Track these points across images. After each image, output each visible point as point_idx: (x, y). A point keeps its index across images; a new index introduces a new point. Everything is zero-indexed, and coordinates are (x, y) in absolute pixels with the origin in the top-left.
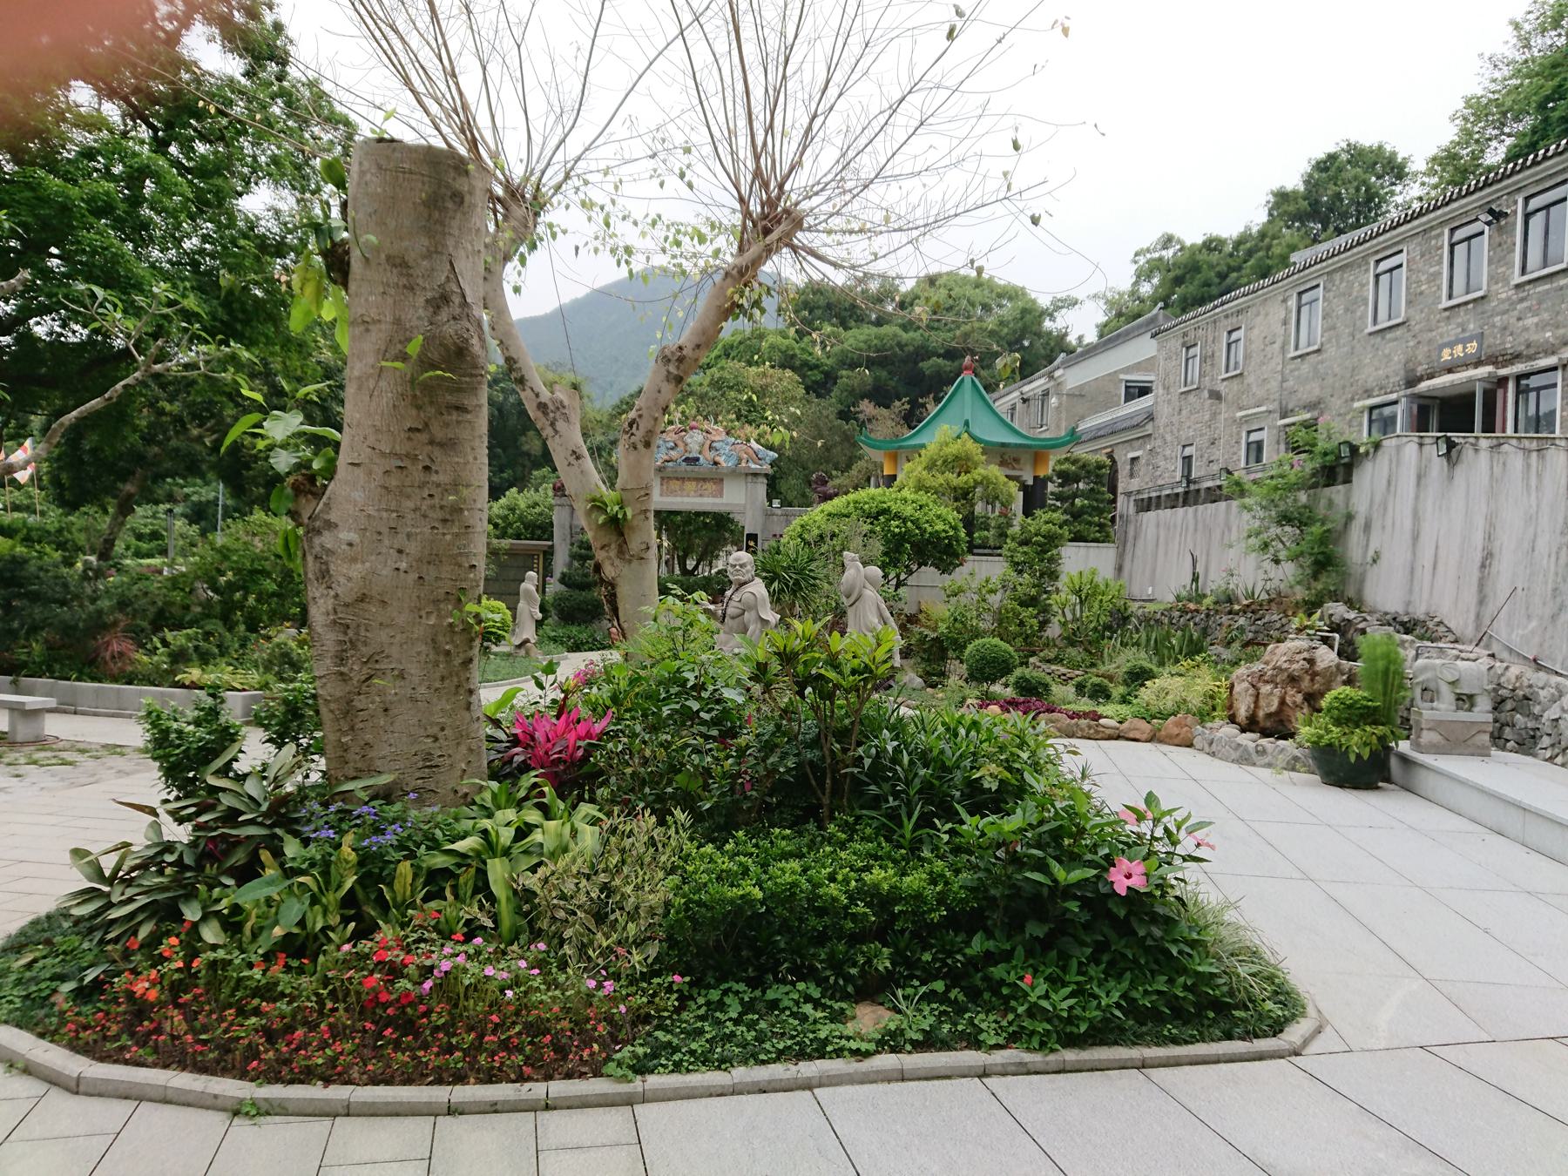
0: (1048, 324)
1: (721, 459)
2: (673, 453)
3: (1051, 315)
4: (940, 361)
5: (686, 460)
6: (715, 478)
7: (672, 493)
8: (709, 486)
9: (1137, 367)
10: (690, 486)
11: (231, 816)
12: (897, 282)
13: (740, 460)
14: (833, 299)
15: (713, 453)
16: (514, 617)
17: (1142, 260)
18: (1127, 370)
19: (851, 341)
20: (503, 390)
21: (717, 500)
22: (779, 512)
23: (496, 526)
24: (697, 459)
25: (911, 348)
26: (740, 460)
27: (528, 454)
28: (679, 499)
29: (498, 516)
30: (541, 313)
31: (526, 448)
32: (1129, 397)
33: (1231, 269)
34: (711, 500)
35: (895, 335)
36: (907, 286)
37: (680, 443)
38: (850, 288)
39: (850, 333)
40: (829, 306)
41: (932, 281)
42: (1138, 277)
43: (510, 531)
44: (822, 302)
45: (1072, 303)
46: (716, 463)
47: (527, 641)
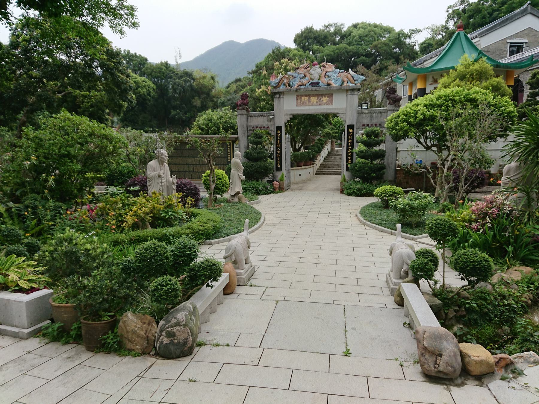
0: (407, 41)
1: (332, 82)
2: (304, 81)
3: (409, 37)
4: (364, 58)
5: (312, 84)
6: (329, 92)
7: (304, 104)
8: (325, 99)
9: (516, 35)
10: (314, 99)
11: (494, 328)
12: (342, 27)
13: (343, 82)
14: (317, 35)
15: (327, 79)
16: (229, 179)
17: (451, 11)
18: (511, 37)
19: (327, 51)
20: (185, 81)
21: (329, 107)
22: (366, 111)
23: (202, 129)
24: (318, 83)
25: (352, 53)
26: (343, 82)
27: (196, 107)
28: (307, 107)
29: (203, 124)
30: (192, 59)
31: (195, 104)
32: (512, 53)
33: (494, 11)
34: (325, 107)
35: (346, 48)
36: (345, 29)
37: (307, 74)
38: (323, 31)
39: (326, 48)
40: (315, 38)
41: (355, 26)
42: (448, 18)
43: (210, 131)
44: (313, 36)
45: (419, 31)
46: (329, 85)
47: (238, 193)
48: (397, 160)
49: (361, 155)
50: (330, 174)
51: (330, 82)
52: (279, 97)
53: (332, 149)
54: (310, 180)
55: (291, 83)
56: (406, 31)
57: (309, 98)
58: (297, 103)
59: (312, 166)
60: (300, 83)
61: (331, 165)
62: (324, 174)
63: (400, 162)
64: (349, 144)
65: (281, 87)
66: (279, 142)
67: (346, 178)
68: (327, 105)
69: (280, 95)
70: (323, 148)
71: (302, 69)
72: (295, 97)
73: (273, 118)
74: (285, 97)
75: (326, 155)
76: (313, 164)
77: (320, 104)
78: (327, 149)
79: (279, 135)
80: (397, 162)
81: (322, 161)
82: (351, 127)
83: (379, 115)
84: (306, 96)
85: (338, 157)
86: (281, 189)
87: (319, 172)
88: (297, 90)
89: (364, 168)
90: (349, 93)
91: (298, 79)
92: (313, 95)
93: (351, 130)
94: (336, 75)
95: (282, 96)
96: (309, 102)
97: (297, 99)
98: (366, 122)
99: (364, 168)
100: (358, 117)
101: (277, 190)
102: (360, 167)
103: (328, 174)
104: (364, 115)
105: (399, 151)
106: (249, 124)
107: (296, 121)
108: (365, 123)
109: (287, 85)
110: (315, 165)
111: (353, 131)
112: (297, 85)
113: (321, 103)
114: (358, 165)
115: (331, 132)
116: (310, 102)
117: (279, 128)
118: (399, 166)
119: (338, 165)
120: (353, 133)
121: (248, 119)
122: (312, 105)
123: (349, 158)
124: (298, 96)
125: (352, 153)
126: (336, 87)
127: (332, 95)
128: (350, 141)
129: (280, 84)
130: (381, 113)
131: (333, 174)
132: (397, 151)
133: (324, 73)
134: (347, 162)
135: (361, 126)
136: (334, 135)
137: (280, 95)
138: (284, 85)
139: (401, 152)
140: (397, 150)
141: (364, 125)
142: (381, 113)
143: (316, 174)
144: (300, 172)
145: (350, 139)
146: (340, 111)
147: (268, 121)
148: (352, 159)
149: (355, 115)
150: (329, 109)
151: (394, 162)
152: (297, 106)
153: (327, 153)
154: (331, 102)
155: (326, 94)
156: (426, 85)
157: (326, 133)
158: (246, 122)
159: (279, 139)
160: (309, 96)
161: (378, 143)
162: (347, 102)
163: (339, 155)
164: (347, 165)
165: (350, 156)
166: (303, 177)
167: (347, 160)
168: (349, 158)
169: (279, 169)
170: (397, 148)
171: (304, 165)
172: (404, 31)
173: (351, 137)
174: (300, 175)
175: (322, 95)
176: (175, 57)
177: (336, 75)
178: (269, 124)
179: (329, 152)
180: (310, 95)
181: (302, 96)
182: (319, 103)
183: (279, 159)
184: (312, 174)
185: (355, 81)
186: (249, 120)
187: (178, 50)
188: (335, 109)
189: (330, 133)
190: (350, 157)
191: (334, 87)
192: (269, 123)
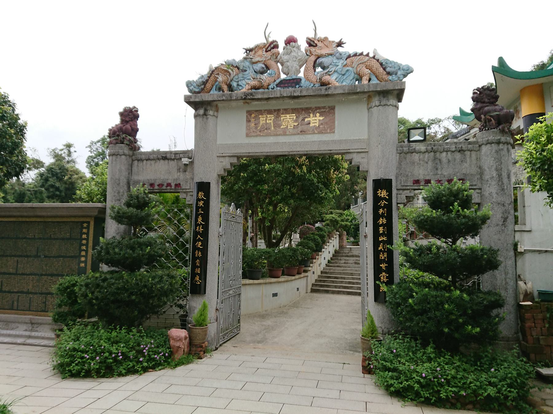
1: (333, 79)
8: (315, 120)
10: (289, 120)
34: (316, 138)
48: (518, 277)
49: (419, 260)
50: (339, 293)
51: (326, 78)
52: (205, 114)
53: (341, 247)
54: (295, 305)
55: (234, 84)
56: (425, 121)
57: (278, 117)
58: (248, 128)
59: (303, 275)
60: (254, 83)
61: (340, 273)
62: (327, 292)
63: (529, 285)
64: (381, 229)
65: (214, 92)
66: (200, 219)
67: (377, 323)
68: (320, 133)
69: (206, 110)
70: (324, 242)
71: (260, 52)
72: (244, 116)
73: (192, 163)
74: (221, 115)
75: (331, 255)
76: (305, 271)
77: (303, 132)
78: (332, 246)
79: (201, 203)
80: (521, 283)
81: (323, 265)
82: (383, 184)
83: (458, 156)
84: (270, 112)
85: (351, 260)
86: (196, 350)
87: (320, 287)
88: (247, 99)
89: (439, 305)
90: (375, 101)
91: (250, 73)
92: (286, 111)
93: (383, 194)
94: (341, 63)
95: (211, 113)
96: (277, 125)
97: (248, 121)
98: (421, 173)
99: (439, 305)
100: (400, 163)
101: (178, 356)
102: (425, 300)
103: (333, 292)
104: (416, 157)
105: (521, 253)
106: (135, 177)
107: (266, 187)
108: (421, 177)
109: (225, 87)
110: (309, 274)
111: (390, 195)
112: (247, 87)
113: (305, 128)
114: (418, 293)
115: (339, 219)
116: (279, 126)
117: (204, 187)
118: (528, 296)
119: (352, 274)
120: (390, 200)
121: (131, 166)
122: (284, 134)
123: (383, 266)
124: (249, 113)
125: (390, 253)
126: (342, 87)
127: (333, 108)
128: (382, 221)
129: (208, 85)
130: (461, 151)
131: (344, 293)
132: (517, 254)
133: (313, 58)
134: (377, 277)
135: (410, 183)
136: (343, 223)
137: (206, 110)
138: (220, 89)
139: (528, 256)
140: (515, 249)
141: (417, 182)
142: (461, 151)
143: (313, 291)
144: (276, 289)
145: (382, 216)
146: (353, 147)
147: (179, 170)
148: (390, 270)
149: (394, 158)
150: (325, 142)
151: (512, 283)
152: (247, 135)
153: (332, 251)
154: (328, 127)
155: (317, 108)
156: (543, 106)
157: (331, 220)
158: (125, 173)
159: (204, 211)
160: (277, 112)
161: (473, 228)
162: (369, 124)
163: (353, 256)
164: (377, 288)
165: (383, 261)
166: (283, 299)
167: (377, 271)
168: (383, 266)
169: (198, 289)
170: (515, 245)
171: (283, 274)
172: (423, 120)
173: (383, 211)
174: (275, 295)
175: (308, 110)
176: (169, 146)
177: (341, 63)
178: (181, 177)
179: (336, 251)
180: (279, 110)
181: (260, 112)
182: (300, 129)
183: (200, 264)
184: (302, 291)
185: (389, 73)
186: (135, 168)
187: (173, 139)
188: (340, 142)
189: (337, 222)
190: (383, 264)
191: (336, 88)
192: (182, 176)
